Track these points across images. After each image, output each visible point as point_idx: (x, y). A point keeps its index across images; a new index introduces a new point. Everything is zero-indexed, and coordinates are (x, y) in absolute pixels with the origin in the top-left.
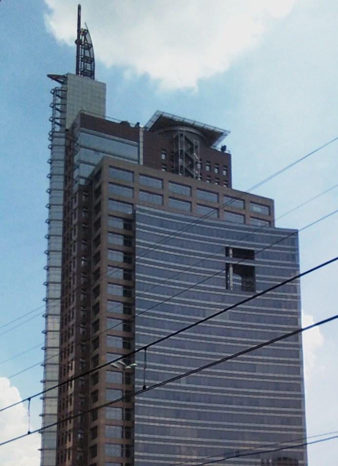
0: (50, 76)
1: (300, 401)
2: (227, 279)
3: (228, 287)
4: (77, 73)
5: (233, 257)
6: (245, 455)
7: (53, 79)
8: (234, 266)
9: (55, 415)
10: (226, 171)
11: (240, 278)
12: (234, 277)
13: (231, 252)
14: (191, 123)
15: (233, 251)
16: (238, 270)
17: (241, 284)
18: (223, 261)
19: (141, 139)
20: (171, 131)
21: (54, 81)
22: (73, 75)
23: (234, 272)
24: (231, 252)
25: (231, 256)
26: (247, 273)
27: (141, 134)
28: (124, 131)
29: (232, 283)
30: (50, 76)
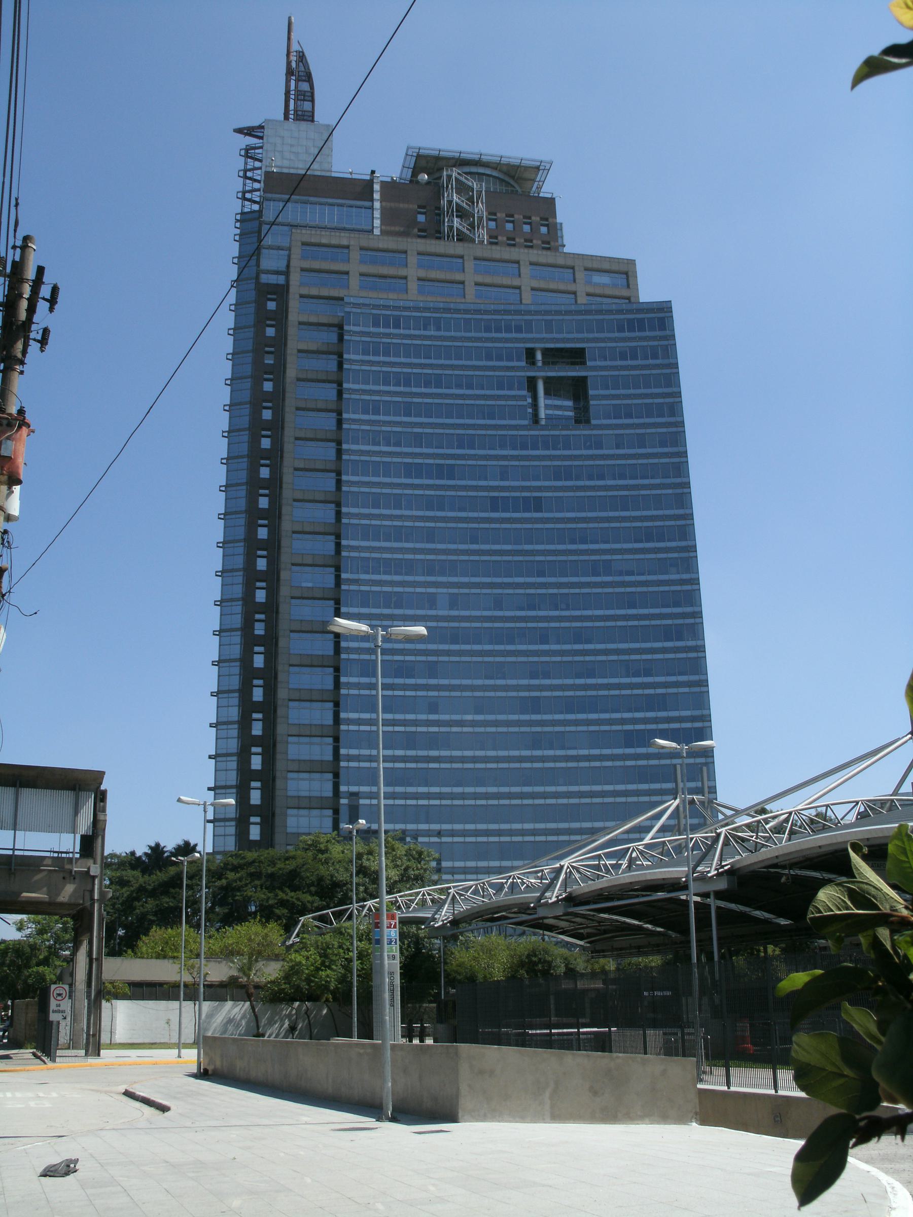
0: (239, 131)
1: (693, 624)
2: (535, 405)
3: (536, 419)
4: (286, 117)
5: (544, 363)
6: (874, 887)
7: (246, 134)
8: (548, 381)
9: (238, 600)
10: (547, 225)
11: (570, 403)
12: (549, 402)
13: (539, 356)
14: (476, 157)
15: (543, 355)
16: (554, 387)
17: (571, 414)
18: (523, 374)
19: (377, 196)
20: (505, 173)
21: (247, 137)
22: (280, 121)
23: (547, 393)
24: (539, 356)
25: (540, 364)
26: (578, 390)
27: (377, 187)
28: (360, 190)
29: (542, 414)
30: (239, 131)
